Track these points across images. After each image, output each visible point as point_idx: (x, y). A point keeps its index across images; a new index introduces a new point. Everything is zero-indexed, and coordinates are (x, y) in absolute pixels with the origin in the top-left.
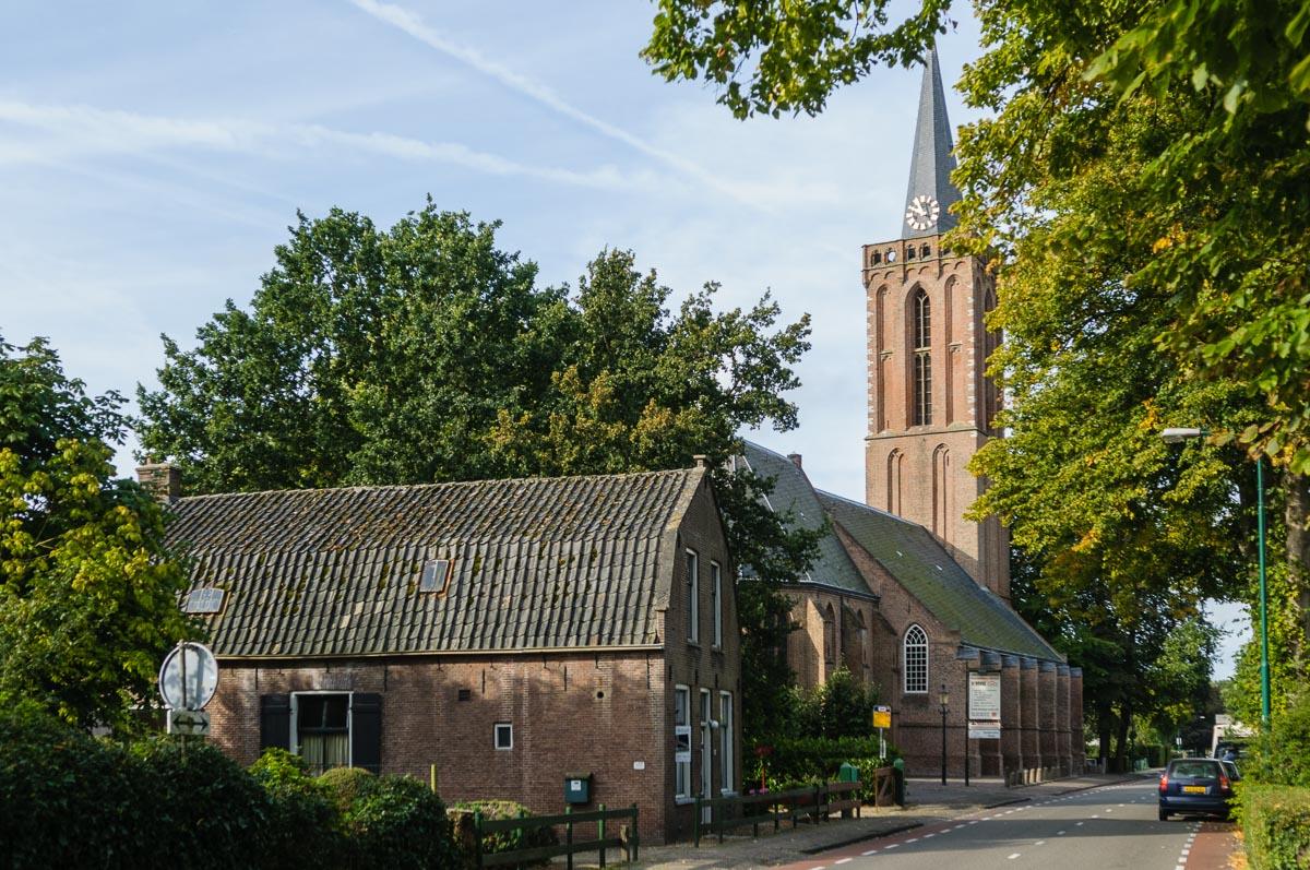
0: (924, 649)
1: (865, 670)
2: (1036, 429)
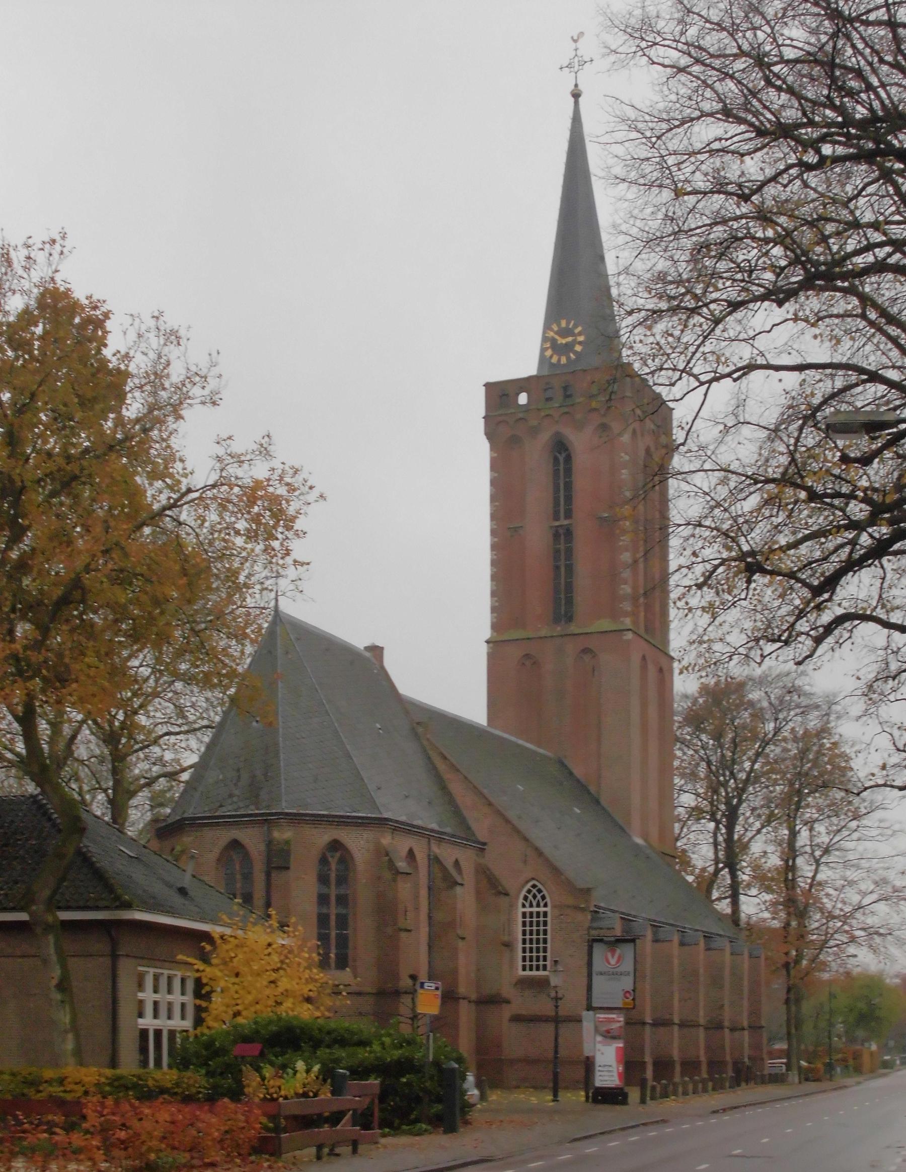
0: (524, 906)
1: (461, 944)
2: (807, 634)
